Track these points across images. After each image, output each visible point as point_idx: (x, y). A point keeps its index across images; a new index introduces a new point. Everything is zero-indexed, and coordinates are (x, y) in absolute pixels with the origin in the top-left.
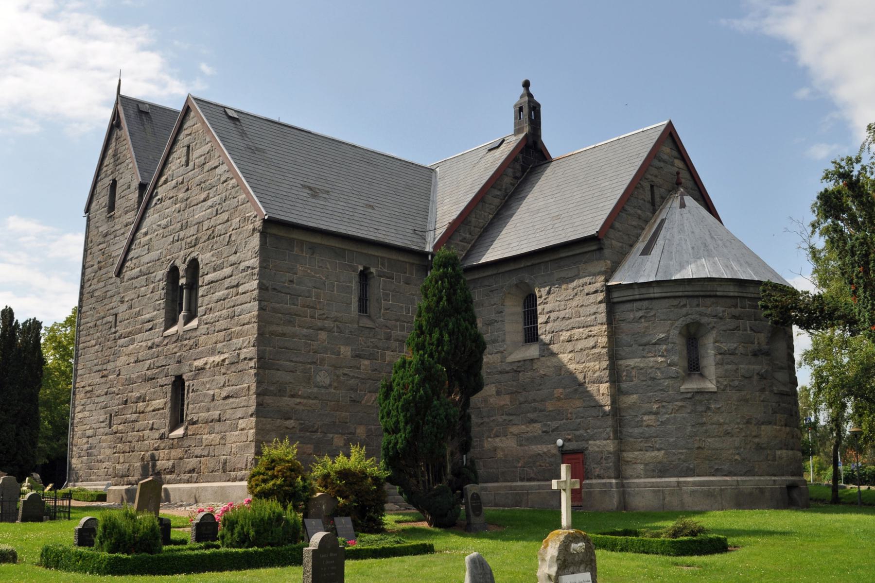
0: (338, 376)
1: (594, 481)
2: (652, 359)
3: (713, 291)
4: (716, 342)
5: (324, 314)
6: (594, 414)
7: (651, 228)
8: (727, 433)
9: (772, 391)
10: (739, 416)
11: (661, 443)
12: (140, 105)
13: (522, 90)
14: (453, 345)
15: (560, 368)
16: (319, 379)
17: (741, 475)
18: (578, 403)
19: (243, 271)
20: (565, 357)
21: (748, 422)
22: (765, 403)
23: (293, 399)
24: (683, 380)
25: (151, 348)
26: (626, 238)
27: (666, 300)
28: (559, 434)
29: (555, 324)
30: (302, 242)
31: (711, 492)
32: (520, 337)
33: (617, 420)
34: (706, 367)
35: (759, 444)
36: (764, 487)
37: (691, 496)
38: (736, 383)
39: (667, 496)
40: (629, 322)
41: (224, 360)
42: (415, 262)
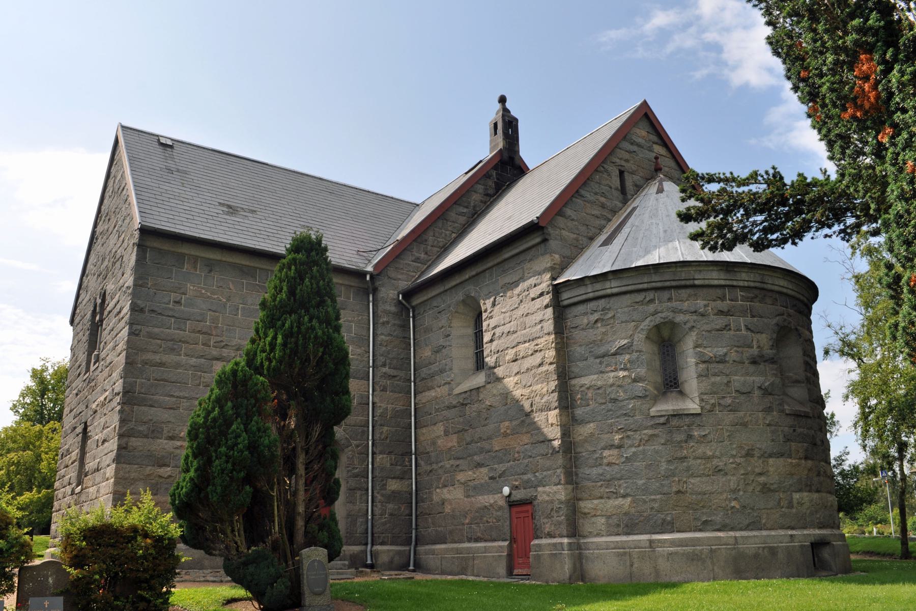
1: (544, 541)
2: (612, 374)
3: (690, 279)
4: (696, 347)
5: (222, 341)
6: (542, 452)
8: (718, 471)
9: (783, 411)
10: (734, 446)
11: (627, 487)
13: (498, 106)
14: (288, 351)
15: (506, 395)
17: (741, 529)
18: (526, 439)
20: (510, 382)
21: (749, 454)
22: (773, 428)
23: (173, 442)
24: (655, 400)
26: (582, 229)
27: (628, 296)
28: (506, 480)
29: (500, 341)
30: (195, 259)
31: (697, 555)
32: (471, 364)
33: (571, 458)
34: (686, 381)
35: (766, 484)
36: (776, 545)
37: (668, 560)
38: (729, 401)
39: (635, 560)
40: (583, 329)
42: (353, 284)
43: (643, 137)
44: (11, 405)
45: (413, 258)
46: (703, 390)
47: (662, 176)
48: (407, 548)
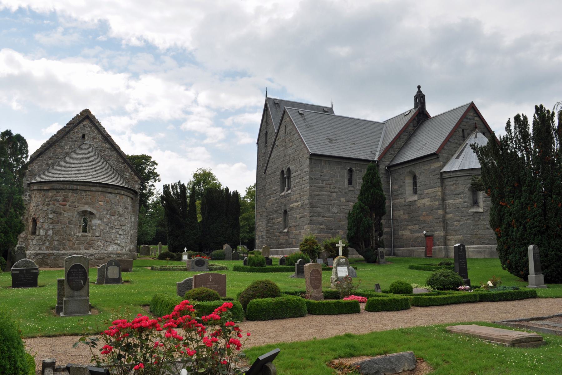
0: (340, 209)
1: (436, 247)
7: (462, 147)
12: (275, 101)
13: (417, 90)
16: (333, 210)
17: (493, 245)
19: (304, 172)
24: (470, 208)
26: (450, 152)
27: (463, 177)
32: (412, 192)
43: (471, 116)
45: (390, 154)
46: (484, 206)
47: (477, 130)
48: (390, 249)
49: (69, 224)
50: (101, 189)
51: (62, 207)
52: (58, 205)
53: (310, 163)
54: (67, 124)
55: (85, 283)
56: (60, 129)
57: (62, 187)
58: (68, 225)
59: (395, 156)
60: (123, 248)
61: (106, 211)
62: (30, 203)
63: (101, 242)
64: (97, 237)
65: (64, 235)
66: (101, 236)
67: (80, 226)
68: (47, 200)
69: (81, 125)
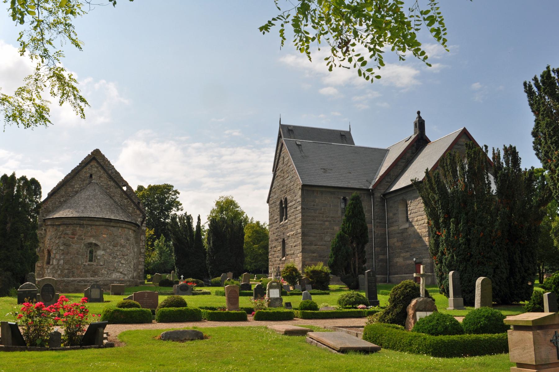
13: (417, 115)
15: (415, 231)
16: (326, 239)
18: (420, 245)
19: (298, 203)
20: (416, 227)
25: (277, 229)
32: (405, 220)
41: (294, 234)
44: (207, 217)
48: (386, 276)
49: (77, 255)
50: (104, 223)
51: (71, 239)
52: (67, 238)
53: (302, 194)
54: (80, 164)
55: (53, 296)
56: (73, 169)
57: (71, 222)
58: (76, 255)
59: (391, 184)
60: (126, 275)
61: (109, 243)
62: (45, 237)
63: (105, 270)
64: (102, 265)
65: (72, 264)
66: (105, 264)
67: (87, 256)
68: (59, 234)
69: (89, 166)
